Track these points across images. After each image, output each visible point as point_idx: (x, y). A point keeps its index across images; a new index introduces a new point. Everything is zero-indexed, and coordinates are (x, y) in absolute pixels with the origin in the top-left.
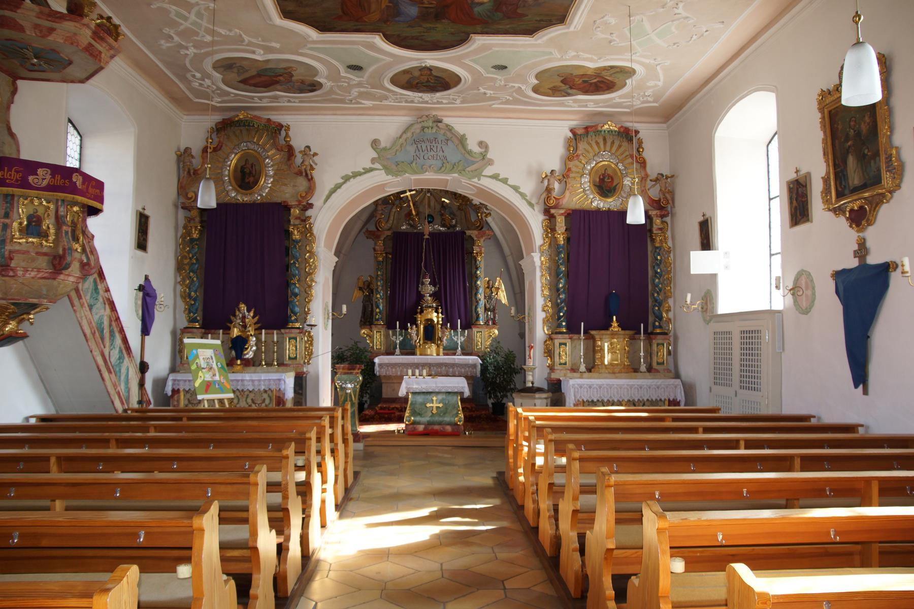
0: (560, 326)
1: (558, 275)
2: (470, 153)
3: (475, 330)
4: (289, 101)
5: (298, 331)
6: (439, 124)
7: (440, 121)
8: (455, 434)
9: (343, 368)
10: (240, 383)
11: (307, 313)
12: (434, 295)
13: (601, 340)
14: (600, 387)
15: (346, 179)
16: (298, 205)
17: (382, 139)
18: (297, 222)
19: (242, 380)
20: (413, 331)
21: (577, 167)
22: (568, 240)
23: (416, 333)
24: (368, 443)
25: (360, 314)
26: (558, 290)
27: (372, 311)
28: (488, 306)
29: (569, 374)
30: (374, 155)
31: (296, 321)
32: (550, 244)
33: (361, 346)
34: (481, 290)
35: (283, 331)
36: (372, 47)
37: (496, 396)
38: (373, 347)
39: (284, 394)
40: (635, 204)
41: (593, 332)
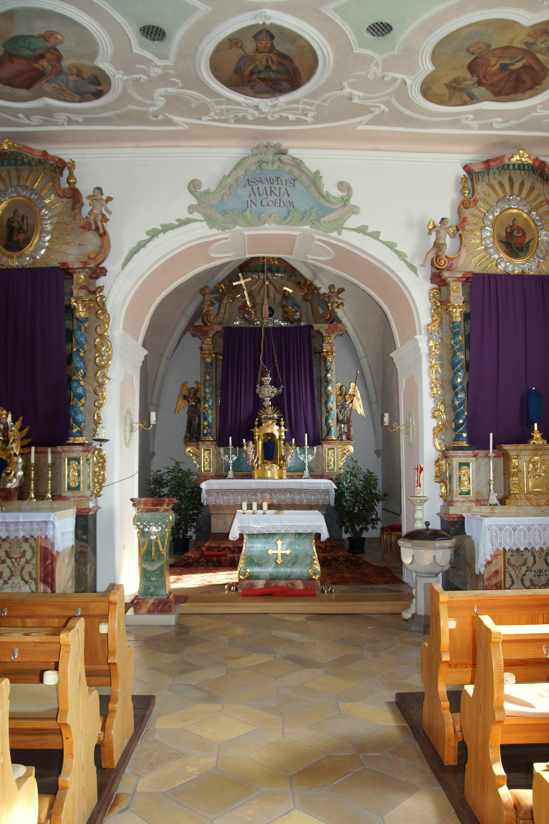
1: (453, 365)
2: (326, 197)
3: (326, 446)
4: (70, 122)
5: (81, 448)
6: (283, 157)
7: (284, 153)
8: (308, 593)
11: (97, 423)
12: (277, 402)
14: (529, 529)
15: (154, 234)
16: (84, 268)
17: (203, 180)
18: (82, 293)
20: (249, 448)
22: (466, 316)
23: (253, 451)
26: (454, 387)
27: (199, 424)
28: (341, 417)
29: (476, 509)
32: (441, 323)
33: (184, 467)
34: (333, 398)
35: (59, 448)
37: (354, 530)
38: (200, 469)
39: (53, 544)
41: (506, 447)
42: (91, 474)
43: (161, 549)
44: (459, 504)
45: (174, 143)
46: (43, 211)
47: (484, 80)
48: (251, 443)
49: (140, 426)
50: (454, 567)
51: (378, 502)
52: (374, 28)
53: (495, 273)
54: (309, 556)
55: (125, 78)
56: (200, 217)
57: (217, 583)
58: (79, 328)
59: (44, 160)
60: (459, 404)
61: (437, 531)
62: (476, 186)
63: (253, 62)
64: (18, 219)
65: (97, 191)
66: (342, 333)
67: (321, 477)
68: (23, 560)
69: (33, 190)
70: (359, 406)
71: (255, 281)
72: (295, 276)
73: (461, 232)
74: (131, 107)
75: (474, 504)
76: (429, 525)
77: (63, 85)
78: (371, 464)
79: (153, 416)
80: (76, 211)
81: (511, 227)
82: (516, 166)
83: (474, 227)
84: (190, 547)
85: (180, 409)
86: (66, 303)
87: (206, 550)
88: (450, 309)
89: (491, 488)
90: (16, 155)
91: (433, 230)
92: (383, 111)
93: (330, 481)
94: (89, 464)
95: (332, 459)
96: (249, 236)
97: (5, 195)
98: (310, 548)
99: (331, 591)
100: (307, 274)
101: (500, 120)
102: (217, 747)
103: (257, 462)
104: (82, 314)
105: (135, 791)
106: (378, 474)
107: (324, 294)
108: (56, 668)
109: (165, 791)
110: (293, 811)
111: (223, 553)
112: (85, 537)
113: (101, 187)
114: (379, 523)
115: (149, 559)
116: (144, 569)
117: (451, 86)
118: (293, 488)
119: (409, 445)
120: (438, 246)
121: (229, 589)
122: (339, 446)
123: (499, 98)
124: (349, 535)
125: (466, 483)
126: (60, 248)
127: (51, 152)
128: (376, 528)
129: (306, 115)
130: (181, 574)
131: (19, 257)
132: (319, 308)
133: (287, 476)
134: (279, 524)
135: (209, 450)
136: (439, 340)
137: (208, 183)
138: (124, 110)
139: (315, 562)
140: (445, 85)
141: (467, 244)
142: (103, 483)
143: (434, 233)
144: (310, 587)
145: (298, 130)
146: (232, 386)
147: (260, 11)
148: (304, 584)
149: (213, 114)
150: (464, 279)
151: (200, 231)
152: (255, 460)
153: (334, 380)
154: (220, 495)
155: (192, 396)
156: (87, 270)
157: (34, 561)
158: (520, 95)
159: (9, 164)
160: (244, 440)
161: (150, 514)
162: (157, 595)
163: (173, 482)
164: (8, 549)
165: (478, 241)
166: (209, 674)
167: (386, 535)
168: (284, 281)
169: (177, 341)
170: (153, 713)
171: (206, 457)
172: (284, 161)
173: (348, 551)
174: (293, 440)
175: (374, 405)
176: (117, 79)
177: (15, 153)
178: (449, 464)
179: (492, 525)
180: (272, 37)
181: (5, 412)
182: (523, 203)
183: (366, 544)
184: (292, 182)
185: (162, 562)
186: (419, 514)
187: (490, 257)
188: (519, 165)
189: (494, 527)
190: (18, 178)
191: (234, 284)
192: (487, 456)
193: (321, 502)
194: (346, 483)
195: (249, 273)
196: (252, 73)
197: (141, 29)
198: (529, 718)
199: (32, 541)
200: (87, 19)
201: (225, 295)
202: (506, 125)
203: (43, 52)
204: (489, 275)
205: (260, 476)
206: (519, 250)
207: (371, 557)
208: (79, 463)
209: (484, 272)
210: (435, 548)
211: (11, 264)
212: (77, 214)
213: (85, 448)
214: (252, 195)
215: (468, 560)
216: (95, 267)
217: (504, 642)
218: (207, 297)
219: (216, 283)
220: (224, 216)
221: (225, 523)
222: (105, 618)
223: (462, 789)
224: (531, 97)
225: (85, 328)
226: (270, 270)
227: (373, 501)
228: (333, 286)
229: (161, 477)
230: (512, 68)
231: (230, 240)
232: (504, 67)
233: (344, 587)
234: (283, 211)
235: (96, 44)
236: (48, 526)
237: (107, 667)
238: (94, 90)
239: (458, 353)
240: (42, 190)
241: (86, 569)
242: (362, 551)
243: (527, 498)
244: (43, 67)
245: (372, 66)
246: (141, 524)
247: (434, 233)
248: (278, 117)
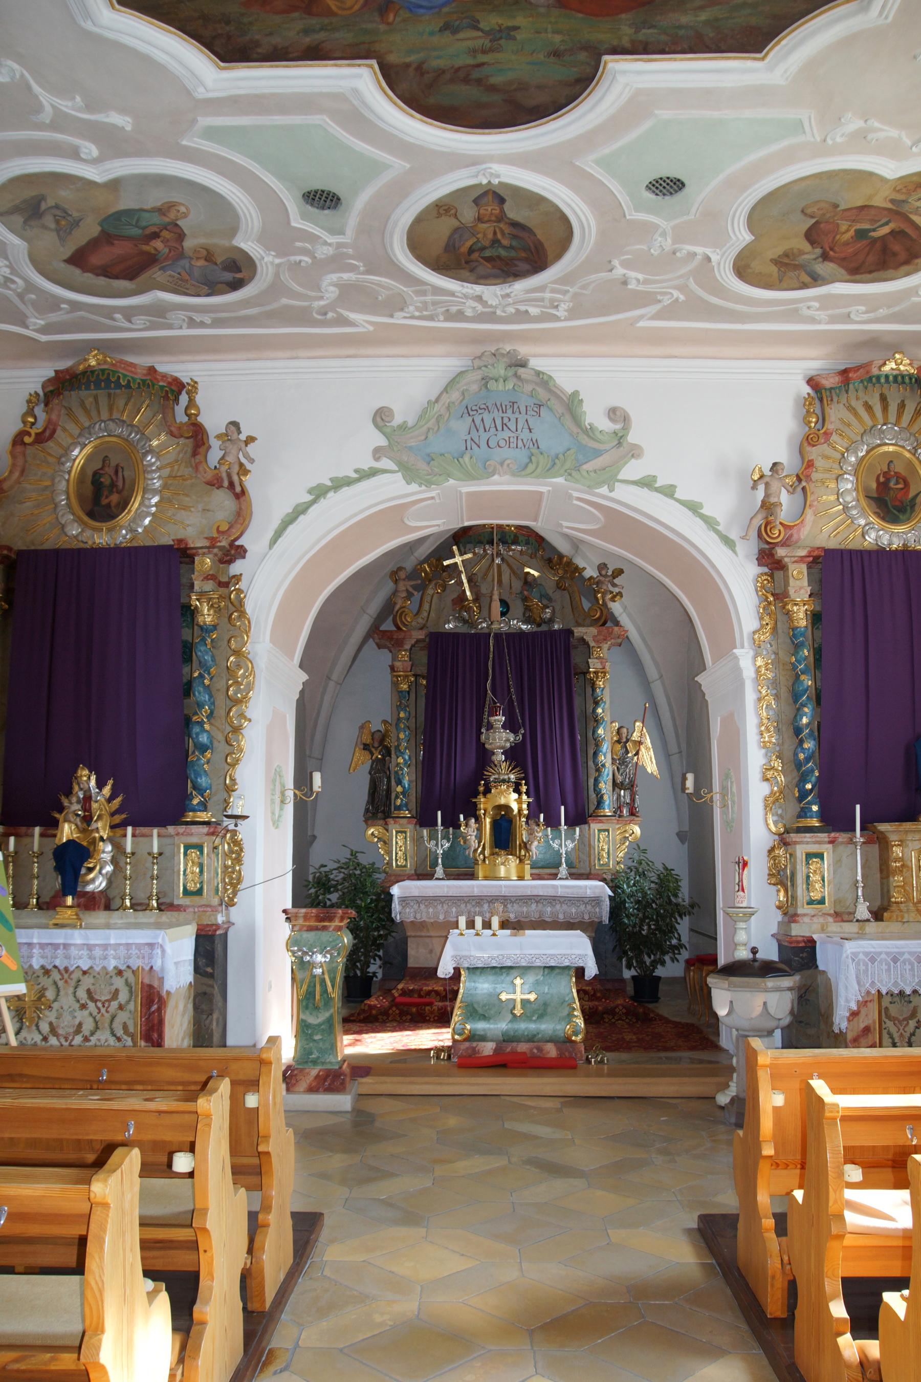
0: (804, 813)
1: (795, 696)
2: (590, 432)
3: (595, 826)
4: (192, 323)
5: (205, 829)
6: (521, 371)
7: (523, 364)
8: (564, 1064)
11: (229, 790)
12: (514, 755)
15: (319, 493)
18: (209, 586)
19: (66, 946)
22: (816, 618)
23: (476, 834)
24: (364, 1090)
25: (365, 797)
26: (798, 731)
27: (389, 790)
28: (619, 779)
29: (834, 927)
30: (381, 441)
31: (204, 807)
32: (774, 629)
33: (364, 860)
34: (606, 747)
35: (171, 829)
36: (355, 118)
37: (641, 963)
38: (389, 863)
39: (161, 980)
41: (883, 827)
42: (220, 871)
43: (330, 989)
44: (806, 919)
45: (351, 351)
46: (149, 458)
47: (831, 253)
48: (473, 820)
49: (295, 795)
50: (801, 1022)
51: (682, 918)
52: (657, 185)
53: (861, 548)
54: (566, 1004)
55: (277, 261)
56: (391, 465)
57: (417, 1047)
58: (203, 640)
59: (151, 380)
60: (805, 758)
61: (773, 962)
62: (827, 409)
63: (474, 235)
64: (110, 471)
65: (233, 428)
66: (619, 641)
67: (588, 876)
68: (114, 1004)
69: (132, 426)
70: (648, 760)
71: (478, 558)
72: (544, 550)
73: (804, 484)
74: (285, 301)
75: (830, 919)
76: (757, 952)
77: (183, 273)
78: (671, 856)
79: (317, 778)
80: (198, 458)
81: (885, 474)
82: (891, 378)
83: (827, 476)
84: (373, 991)
85: (356, 765)
86: (183, 601)
87: (400, 995)
88: (789, 607)
89: (860, 893)
90: (109, 374)
91: (759, 482)
92: (677, 300)
93: (601, 883)
94: (218, 855)
95: (606, 847)
96: (469, 494)
97: (90, 434)
98: (568, 991)
99: (602, 1061)
100: (563, 547)
101: (863, 308)
102: (419, 1289)
103: (483, 852)
104: (208, 619)
105: (297, 1345)
106: (682, 870)
107: (591, 578)
108: (192, 1148)
109: (342, 1346)
110: (534, 1378)
111: (427, 1000)
112: (209, 970)
113: (237, 420)
114: (683, 951)
115: (311, 1005)
116: (303, 1021)
117: (781, 262)
119: (727, 824)
120: (768, 507)
121: (438, 1057)
122: (617, 826)
123: (858, 277)
124: (633, 972)
125: (818, 886)
126: (174, 515)
127: (161, 368)
128: (678, 961)
129: (557, 307)
130: (360, 1032)
131: (110, 530)
132: (583, 599)
133: (531, 875)
134: (518, 952)
135: (405, 832)
136: (773, 657)
137: (405, 408)
138: (275, 306)
139: (576, 1013)
140: (771, 260)
141: (815, 503)
142: (238, 884)
143: (761, 488)
144: (567, 1054)
145: (544, 329)
146: (442, 747)
147: (484, 166)
148: (558, 1049)
149: (411, 308)
150: (811, 559)
151: (391, 488)
153: (607, 719)
154: (422, 906)
155: (376, 745)
156: (216, 550)
157: (131, 1006)
158: (891, 272)
159: (98, 387)
160: (462, 817)
161: (313, 933)
162: (323, 1063)
163: (346, 884)
164: (92, 988)
165: (833, 498)
166: (405, 1184)
167: (694, 971)
168: (525, 558)
169: (352, 654)
170: (320, 1239)
171: (400, 843)
172: (523, 376)
173: (631, 998)
174: (542, 816)
175: (675, 758)
176: (266, 264)
177: (106, 372)
178: (791, 855)
179: (859, 953)
180: (502, 200)
181: (86, 772)
182: (903, 435)
183: (662, 987)
184: (535, 409)
185: (332, 1011)
186: (741, 936)
187: (852, 522)
188: (895, 377)
189: (861, 956)
190: (111, 409)
191: (445, 563)
192: (851, 841)
193: (586, 917)
194: (629, 886)
195: (469, 546)
196: (471, 251)
197: (304, 195)
198: (887, 1237)
199: (128, 975)
200: (222, 182)
201: (430, 581)
202: (872, 315)
203: (157, 230)
204: (851, 552)
205: (488, 874)
206: (899, 511)
207: (669, 1008)
208: (202, 852)
209: (842, 547)
210: (766, 990)
211: (97, 541)
212: (201, 462)
213: (212, 830)
214: (474, 431)
215: (823, 1011)
216: (227, 546)
217: (844, 1119)
218: (402, 586)
219: (415, 562)
220: (429, 463)
221: (431, 951)
222: (253, 1085)
223: (791, 1351)
224: (907, 274)
225: (212, 640)
226: (503, 541)
227: (672, 915)
228: (605, 565)
229: (326, 876)
230: (875, 234)
231: (438, 501)
232: (861, 234)
233: (624, 1056)
234: (521, 455)
235: (235, 217)
236: (154, 952)
237: (256, 1161)
238: (231, 279)
239: (803, 677)
240: (147, 425)
241: (212, 1020)
242: (655, 998)
243: (917, 910)
244: (155, 249)
245: (656, 236)
246: (299, 950)
247: (761, 488)
248: (513, 311)
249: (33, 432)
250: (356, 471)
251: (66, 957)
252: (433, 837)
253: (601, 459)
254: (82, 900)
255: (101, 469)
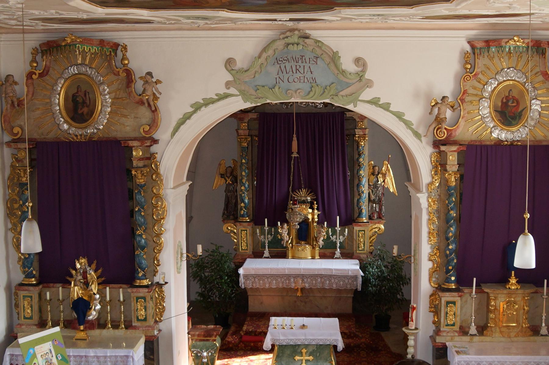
0: (448, 280)
1: (447, 221)
5: (146, 290)
6: (306, 40)
9: (198, 335)
10: (83, 359)
13: (495, 299)
15: (197, 107)
18: (141, 164)
20: (284, 231)
21: (475, 88)
26: (447, 239)
27: (236, 204)
28: (373, 197)
31: (145, 277)
33: (223, 251)
34: (364, 181)
40: (525, 244)
44: (444, 334)
48: (286, 225)
56: (236, 92)
64: (81, 94)
75: (457, 334)
81: (507, 97)
87: (245, 334)
112: (152, 357)
118: (323, 273)
120: (439, 120)
135: (246, 230)
136: (438, 197)
146: (268, 169)
152: (290, 241)
154: (256, 280)
155: (228, 175)
160: (279, 223)
174: (326, 223)
184: (315, 60)
193: (349, 286)
206: (512, 119)
249: (37, 72)
250: (217, 95)
251: (86, 362)
252: (262, 233)
253: (350, 88)
254: (87, 325)
255: (77, 93)
